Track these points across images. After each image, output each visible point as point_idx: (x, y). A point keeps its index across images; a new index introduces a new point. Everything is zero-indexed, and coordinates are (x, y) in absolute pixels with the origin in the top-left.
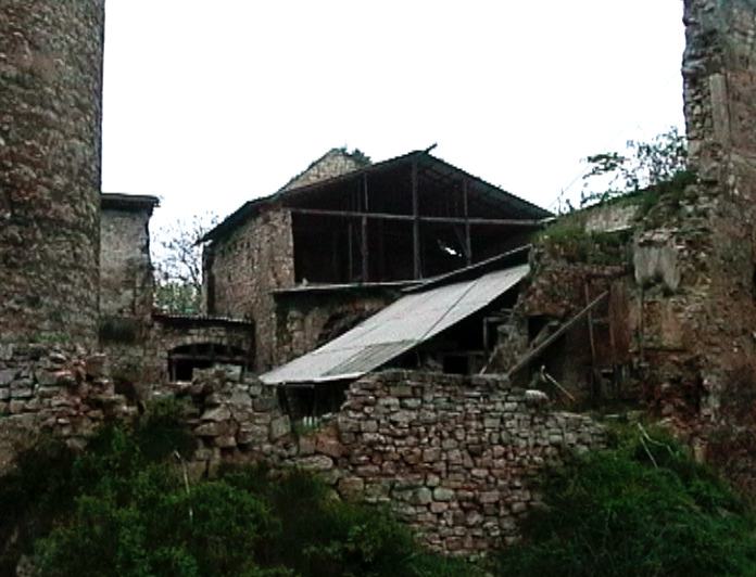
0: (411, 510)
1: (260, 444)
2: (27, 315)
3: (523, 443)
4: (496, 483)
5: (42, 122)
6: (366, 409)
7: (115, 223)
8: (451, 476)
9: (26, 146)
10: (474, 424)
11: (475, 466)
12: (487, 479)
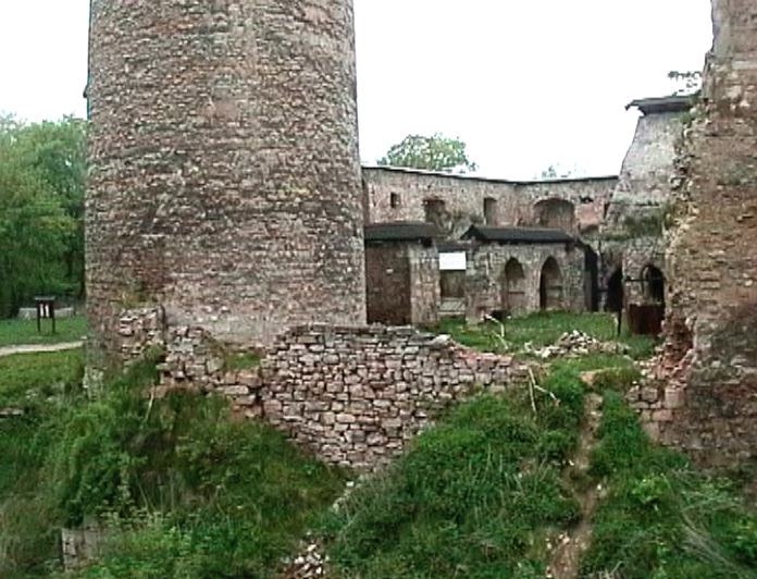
0: (319, 427)
1: (200, 376)
2: (223, 277)
3: (427, 381)
4: (398, 413)
5: (227, 148)
6: (280, 353)
7: (669, 124)
8: (352, 404)
9: (215, 168)
10: (374, 364)
11: (377, 398)
12: (388, 408)
